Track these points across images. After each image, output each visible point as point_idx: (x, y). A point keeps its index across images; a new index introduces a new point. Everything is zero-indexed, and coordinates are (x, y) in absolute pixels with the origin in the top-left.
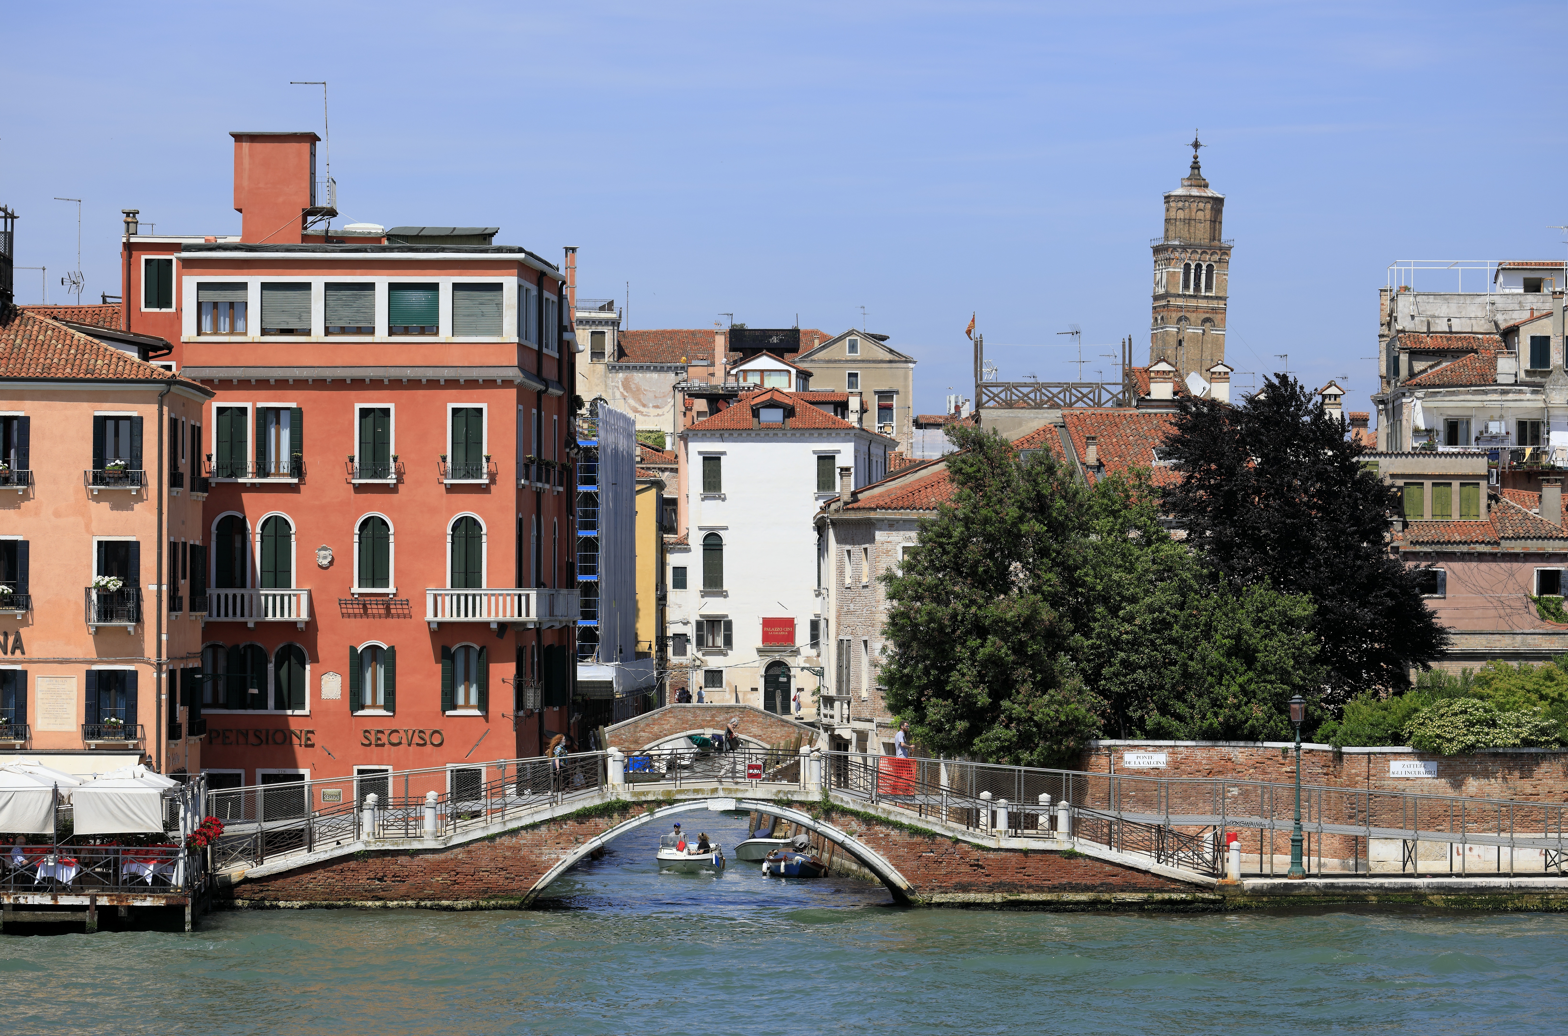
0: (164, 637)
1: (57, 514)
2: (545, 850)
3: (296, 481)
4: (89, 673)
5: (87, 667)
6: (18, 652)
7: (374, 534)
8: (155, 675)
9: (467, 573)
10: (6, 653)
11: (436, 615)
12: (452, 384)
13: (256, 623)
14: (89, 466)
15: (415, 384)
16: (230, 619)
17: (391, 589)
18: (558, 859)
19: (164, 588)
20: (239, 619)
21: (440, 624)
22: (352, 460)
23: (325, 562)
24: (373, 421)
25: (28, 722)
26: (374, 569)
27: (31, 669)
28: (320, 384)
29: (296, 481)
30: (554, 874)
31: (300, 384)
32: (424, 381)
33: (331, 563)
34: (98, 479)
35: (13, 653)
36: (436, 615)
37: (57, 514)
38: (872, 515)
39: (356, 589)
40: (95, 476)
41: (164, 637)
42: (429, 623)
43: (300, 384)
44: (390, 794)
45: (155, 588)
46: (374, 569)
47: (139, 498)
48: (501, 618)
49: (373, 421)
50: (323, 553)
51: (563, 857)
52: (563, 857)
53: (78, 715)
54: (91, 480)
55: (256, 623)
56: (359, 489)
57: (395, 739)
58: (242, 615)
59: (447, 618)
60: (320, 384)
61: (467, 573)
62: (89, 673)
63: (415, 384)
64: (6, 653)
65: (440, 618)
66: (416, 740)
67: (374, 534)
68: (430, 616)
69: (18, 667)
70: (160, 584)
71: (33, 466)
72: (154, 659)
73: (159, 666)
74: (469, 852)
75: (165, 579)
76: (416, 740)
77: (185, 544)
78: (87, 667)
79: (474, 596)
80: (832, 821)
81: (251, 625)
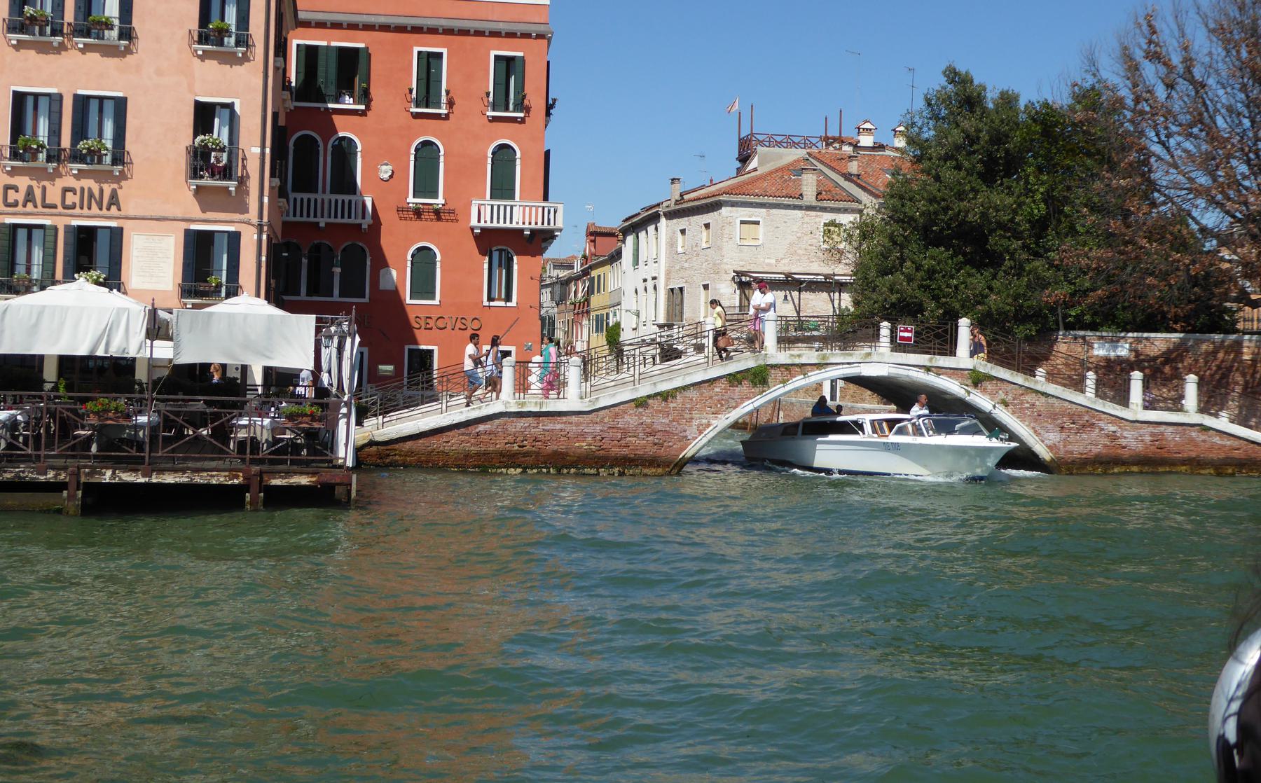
0: (266, 200)
1: (159, 72)
2: (695, 414)
3: (363, 107)
4: (187, 232)
5: (185, 226)
6: (114, 208)
7: (427, 153)
8: (256, 237)
9: (503, 189)
10: (101, 209)
11: (479, 221)
12: (417, 30)
13: (327, 224)
14: (195, 25)
15: (464, 32)
16: (304, 219)
17: (440, 200)
18: (709, 425)
19: (268, 150)
20: (312, 219)
21: (482, 229)
22: (411, 91)
23: (386, 176)
24: (430, 62)
25: (123, 279)
26: (426, 185)
27: (127, 226)
28: (385, 28)
29: (363, 107)
30: (705, 441)
31: (369, 27)
32: (472, 31)
33: (391, 177)
34: (203, 39)
35: (108, 209)
36: (479, 221)
37: (159, 72)
38: (721, 198)
39: (411, 199)
40: (200, 35)
41: (266, 200)
42: (472, 229)
43: (369, 27)
44: (435, 366)
45: (257, 150)
46: (426, 185)
47: (245, 59)
48: (533, 226)
49: (430, 62)
50: (384, 168)
51: (714, 422)
52: (714, 422)
53: (175, 274)
54: (196, 38)
55: (327, 224)
56: (417, 116)
57: (441, 324)
58: (315, 216)
59: (489, 225)
60: (385, 28)
61: (503, 189)
62: (187, 232)
63: (464, 32)
64: (101, 209)
65: (482, 224)
66: (459, 325)
67: (427, 153)
68: (474, 222)
69: (113, 224)
70: (263, 147)
71: (135, 23)
72: (255, 220)
73: (260, 228)
74: (617, 415)
75: (268, 143)
76: (459, 325)
77: (82, 103)
78: (185, 226)
79: (512, 207)
80: (984, 391)
81: (322, 225)
